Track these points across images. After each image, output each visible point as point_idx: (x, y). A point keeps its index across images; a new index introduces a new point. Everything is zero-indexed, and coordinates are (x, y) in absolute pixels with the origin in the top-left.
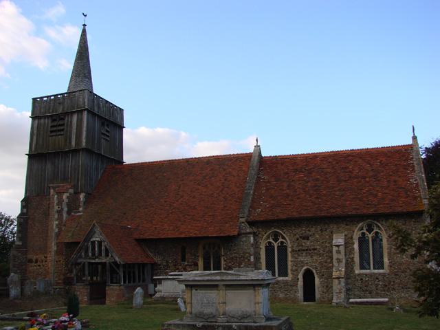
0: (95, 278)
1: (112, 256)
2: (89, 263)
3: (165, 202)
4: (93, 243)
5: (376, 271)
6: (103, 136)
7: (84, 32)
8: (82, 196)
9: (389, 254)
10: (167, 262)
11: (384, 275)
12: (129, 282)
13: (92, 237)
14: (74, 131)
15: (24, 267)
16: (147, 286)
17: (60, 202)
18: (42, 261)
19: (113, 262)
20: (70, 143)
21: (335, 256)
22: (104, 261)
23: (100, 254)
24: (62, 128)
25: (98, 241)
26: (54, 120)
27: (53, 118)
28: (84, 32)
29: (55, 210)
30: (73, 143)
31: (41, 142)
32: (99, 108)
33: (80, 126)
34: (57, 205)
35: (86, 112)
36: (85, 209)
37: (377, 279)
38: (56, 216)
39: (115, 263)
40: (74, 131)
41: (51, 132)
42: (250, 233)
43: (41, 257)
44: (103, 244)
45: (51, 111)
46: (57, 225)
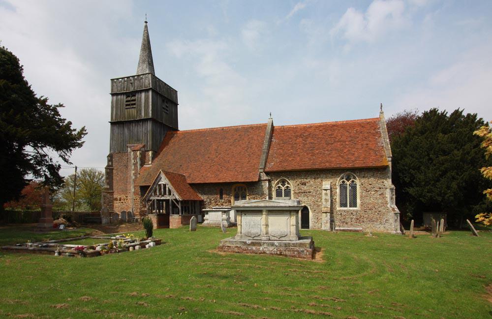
0: (161, 211)
2: (157, 200)
3: (209, 157)
5: (351, 208)
7: (146, 27)
8: (150, 153)
9: (361, 197)
10: (210, 200)
11: (357, 211)
13: (159, 182)
14: (143, 105)
17: (135, 158)
19: (174, 199)
20: (141, 114)
21: (324, 197)
22: (168, 198)
23: (165, 193)
27: (128, 94)
28: (146, 27)
30: (143, 114)
33: (146, 101)
34: (134, 159)
35: (150, 93)
37: (352, 214)
38: (133, 167)
39: (176, 200)
40: (143, 105)
41: (127, 105)
42: (266, 180)
43: (123, 196)
44: (167, 186)
45: (125, 89)
46: (134, 174)
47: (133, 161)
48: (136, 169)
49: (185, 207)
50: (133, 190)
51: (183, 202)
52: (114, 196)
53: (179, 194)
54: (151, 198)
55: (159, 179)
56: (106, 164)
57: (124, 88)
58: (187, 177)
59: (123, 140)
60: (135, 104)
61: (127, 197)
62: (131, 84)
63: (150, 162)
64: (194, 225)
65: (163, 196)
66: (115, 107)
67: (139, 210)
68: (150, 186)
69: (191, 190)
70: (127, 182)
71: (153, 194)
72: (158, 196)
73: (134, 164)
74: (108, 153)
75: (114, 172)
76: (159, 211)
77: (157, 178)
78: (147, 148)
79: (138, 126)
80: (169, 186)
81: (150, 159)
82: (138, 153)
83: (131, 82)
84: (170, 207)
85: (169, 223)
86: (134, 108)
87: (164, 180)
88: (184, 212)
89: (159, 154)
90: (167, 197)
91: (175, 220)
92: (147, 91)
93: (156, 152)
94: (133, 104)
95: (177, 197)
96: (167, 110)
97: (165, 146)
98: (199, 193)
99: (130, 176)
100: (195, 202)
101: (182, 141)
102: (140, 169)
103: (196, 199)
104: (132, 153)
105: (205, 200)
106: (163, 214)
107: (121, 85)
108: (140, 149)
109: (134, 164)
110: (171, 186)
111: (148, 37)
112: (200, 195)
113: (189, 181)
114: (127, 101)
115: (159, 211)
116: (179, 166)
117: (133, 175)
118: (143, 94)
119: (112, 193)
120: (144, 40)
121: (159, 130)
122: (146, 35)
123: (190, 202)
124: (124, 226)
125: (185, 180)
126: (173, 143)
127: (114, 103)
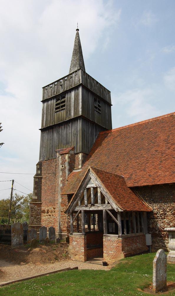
0: (92, 227)
1: (108, 203)
2: (86, 212)
3: (156, 151)
4: (89, 189)
6: (96, 109)
8: (80, 156)
10: (164, 210)
12: (128, 233)
13: (87, 185)
14: (72, 104)
15: (39, 216)
16: (144, 236)
17: (63, 163)
18: (52, 212)
19: (110, 210)
20: (70, 114)
22: (100, 208)
23: (96, 202)
24: (63, 104)
25: (94, 188)
26: (57, 100)
29: (60, 169)
30: (72, 114)
31: (49, 119)
32: (91, 85)
33: (76, 101)
34: (62, 164)
35: (80, 89)
36: (82, 166)
38: (61, 174)
39: (113, 211)
40: (72, 104)
43: (51, 208)
44: (99, 190)
45: (55, 93)
46: (61, 181)
47: (61, 167)
48: (64, 176)
49: (127, 221)
50: (60, 200)
51: (125, 215)
52: (42, 208)
53: (118, 202)
54: (78, 209)
55: (87, 180)
56: (35, 172)
57: (54, 92)
58: (126, 179)
59: (52, 146)
60: (64, 106)
61: (54, 209)
62: (61, 85)
63: (80, 167)
64: (162, 273)
65: (93, 205)
66: (46, 114)
67: (66, 225)
68: (73, 194)
69: (134, 196)
70: (55, 191)
71: (79, 202)
72: (87, 206)
73: (62, 170)
74: (37, 160)
75: (43, 181)
76: (89, 226)
77: (85, 179)
78: (77, 150)
79: (67, 128)
80: (102, 189)
81: (80, 163)
82: (67, 157)
83: (61, 84)
84: (104, 222)
85: (102, 247)
86: (64, 109)
87: (94, 182)
88: (125, 230)
89: (91, 156)
90: (99, 207)
91: (112, 243)
92: (76, 88)
93: (87, 154)
94: (62, 106)
95: (115, 206)
96: (99, 110)
97: (97, 148)
98: (146, 201)
99: (58, 184)
100: (140, 214)
101: (118, 139)
102: (68, 175)
103: (142, 210)
104: (60, 157)
105: (155, 211)
106: (94, 232)
107: (52, 90)
108: (69, 152)
109: (62, 170)
110: (105, 190)
111: (79, 37)
112: (147, 204)
113: (130, 184)
114: (56, 105)
115: (89, 226)
116: (115, 167)
117: (61, 182)
118: (73, 93)
119: (40, 205)
120: (75, 45)
121: (90, 130)
122: (77, 41)
123: (134, 214)
124: (37, 249)
125: (124, 182)
126: (107, 143)
127: (45, 110)
